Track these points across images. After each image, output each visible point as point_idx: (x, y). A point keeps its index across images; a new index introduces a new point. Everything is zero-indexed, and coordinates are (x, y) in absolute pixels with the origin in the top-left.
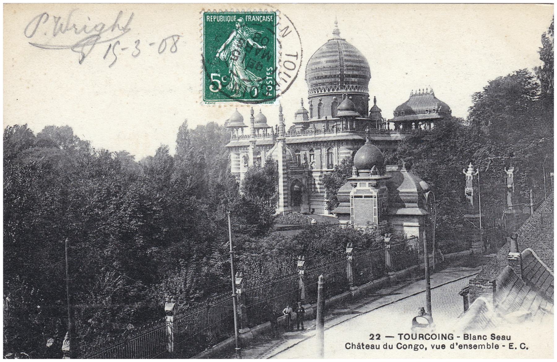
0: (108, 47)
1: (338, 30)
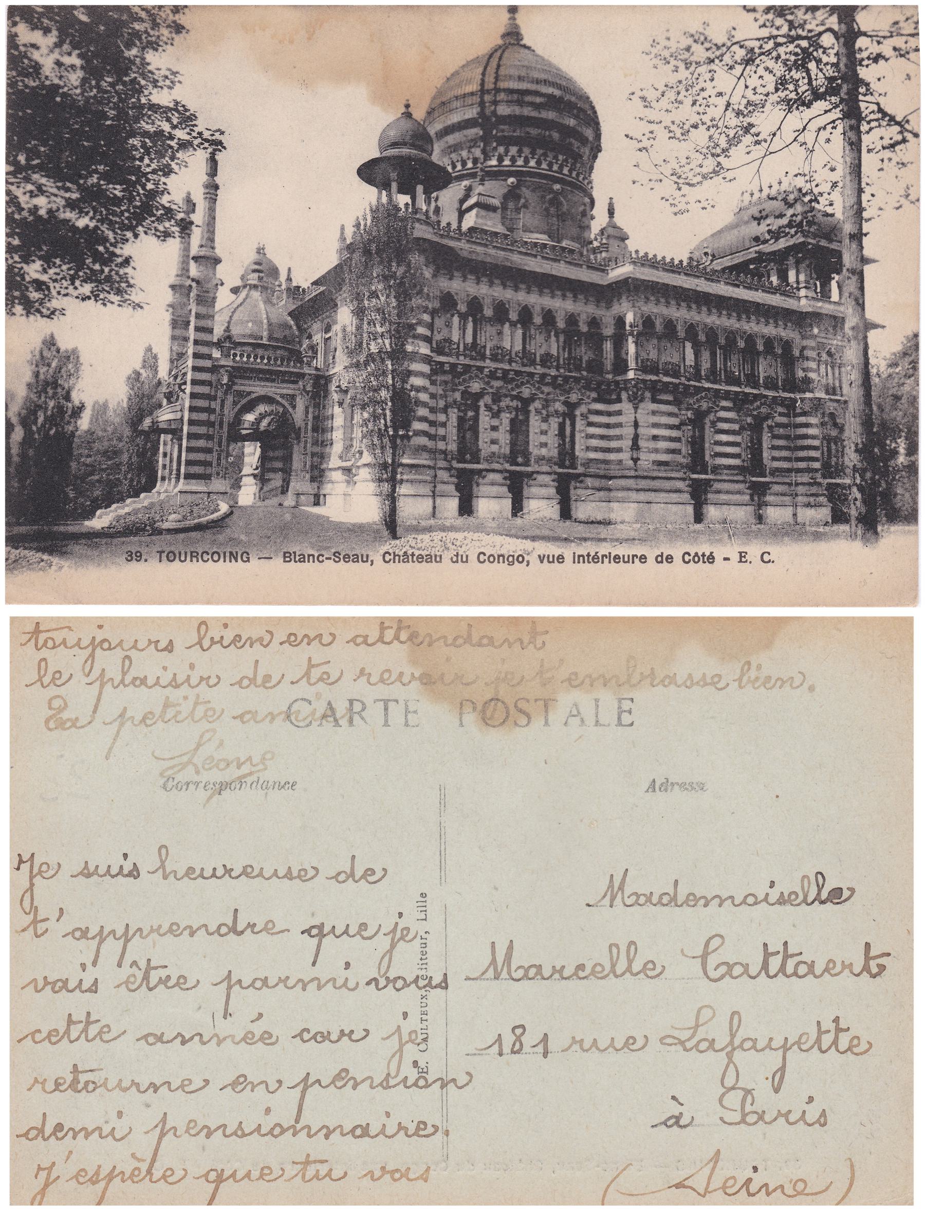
0: (292, 276)
1: (517, 26)
